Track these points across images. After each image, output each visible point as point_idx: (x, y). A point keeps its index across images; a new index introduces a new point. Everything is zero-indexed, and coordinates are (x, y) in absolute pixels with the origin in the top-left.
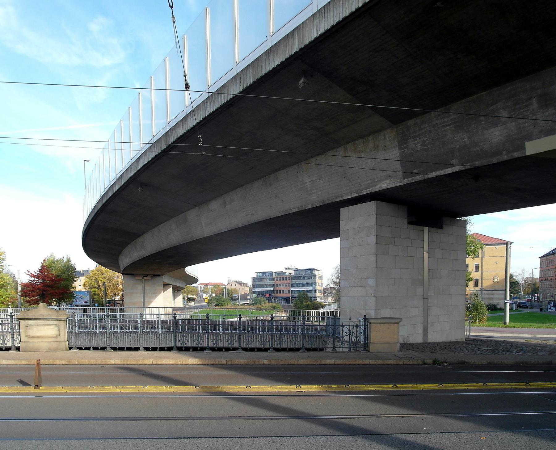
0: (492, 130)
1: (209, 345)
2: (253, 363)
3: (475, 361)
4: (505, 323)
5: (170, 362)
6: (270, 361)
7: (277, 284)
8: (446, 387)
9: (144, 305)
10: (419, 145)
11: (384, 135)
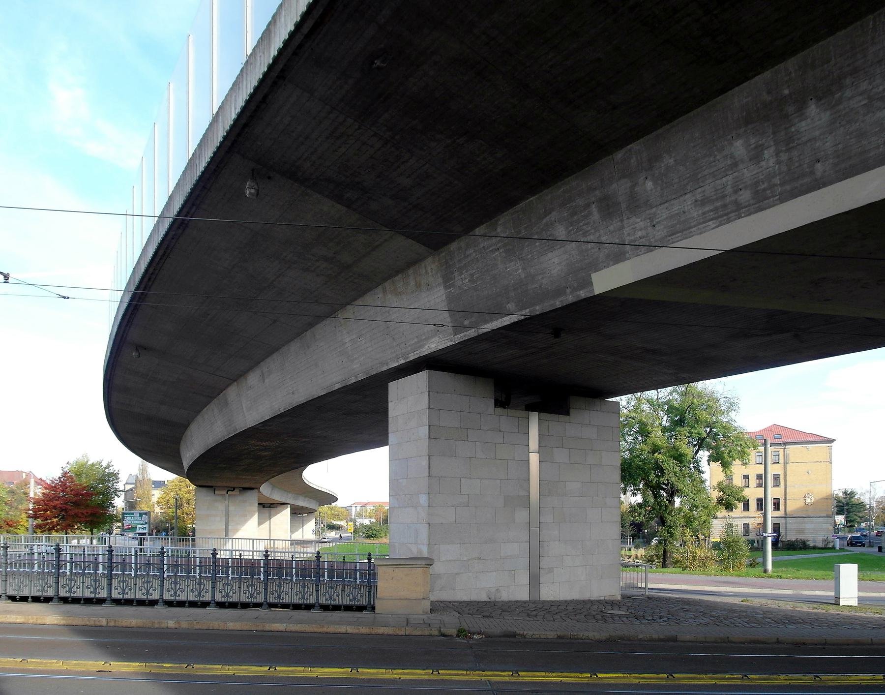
0: (550, 255)
1: (8, 592)
2: (150, 625)
3: (534, 633)
4: (765, 571)
5: (16, 620)
6: (179, 623)
8: (363, 673)
9: (227, 534)
10: (467, 281)
11: (425, 267)
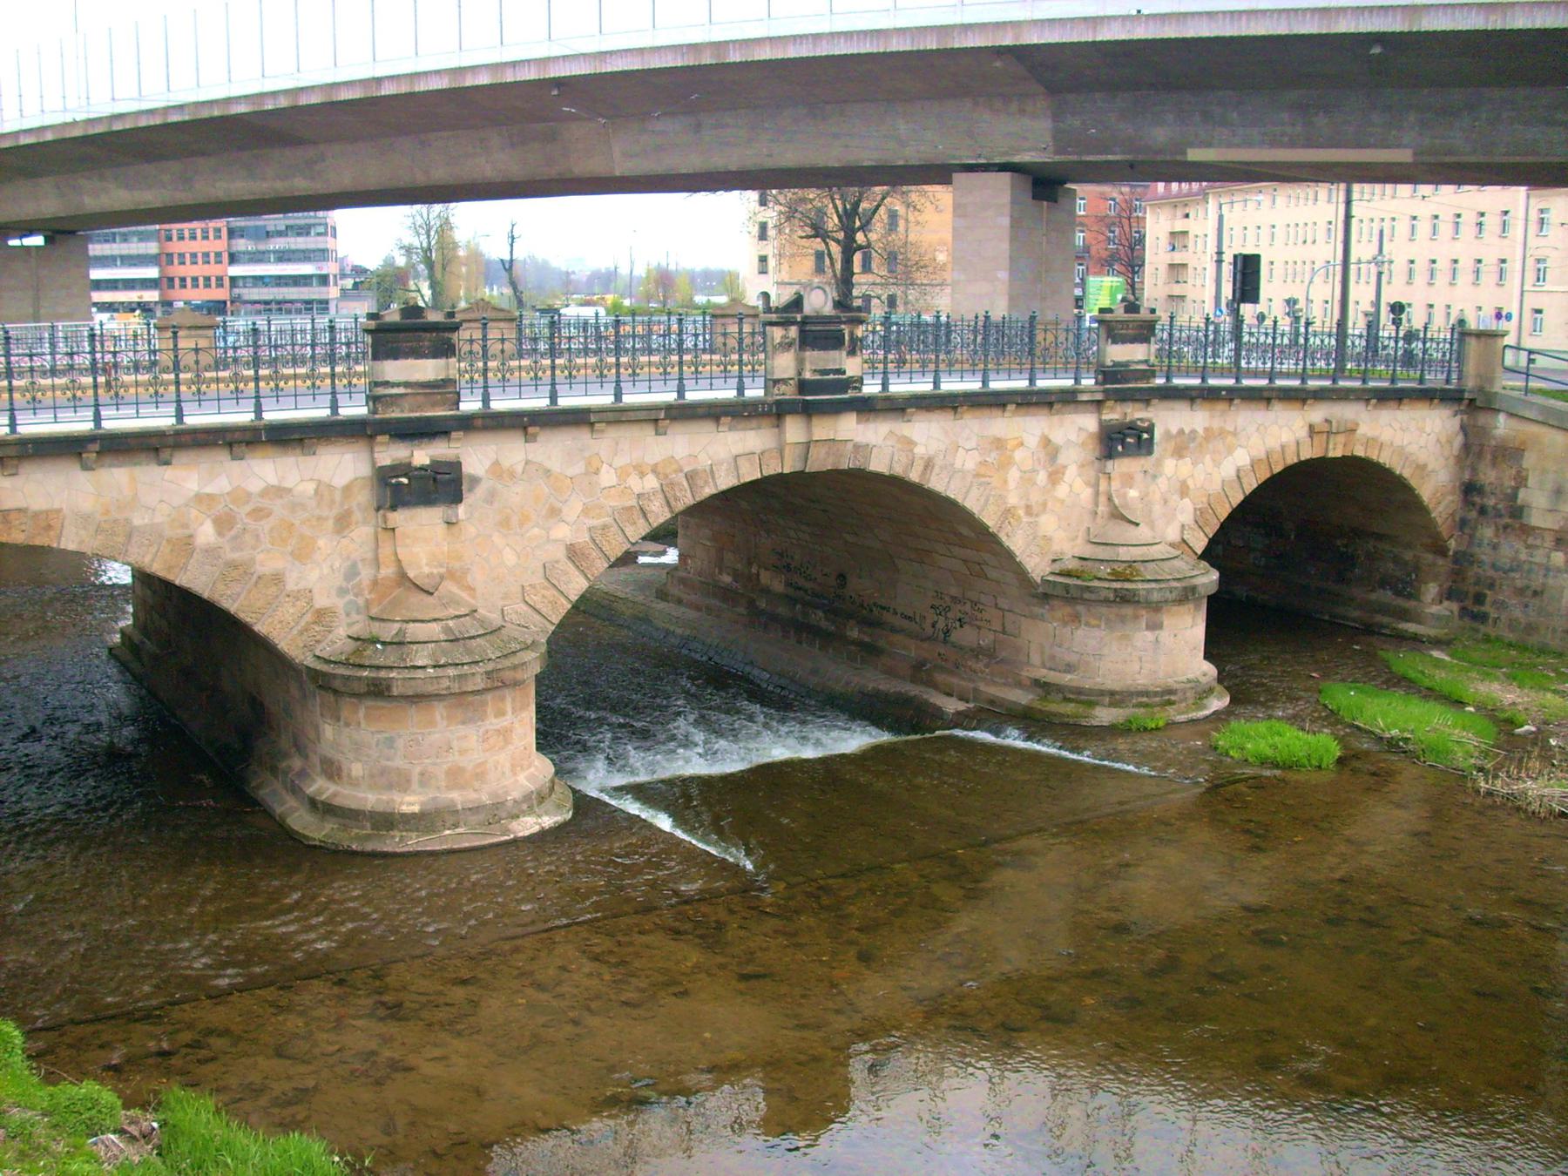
7: (172, 255)
